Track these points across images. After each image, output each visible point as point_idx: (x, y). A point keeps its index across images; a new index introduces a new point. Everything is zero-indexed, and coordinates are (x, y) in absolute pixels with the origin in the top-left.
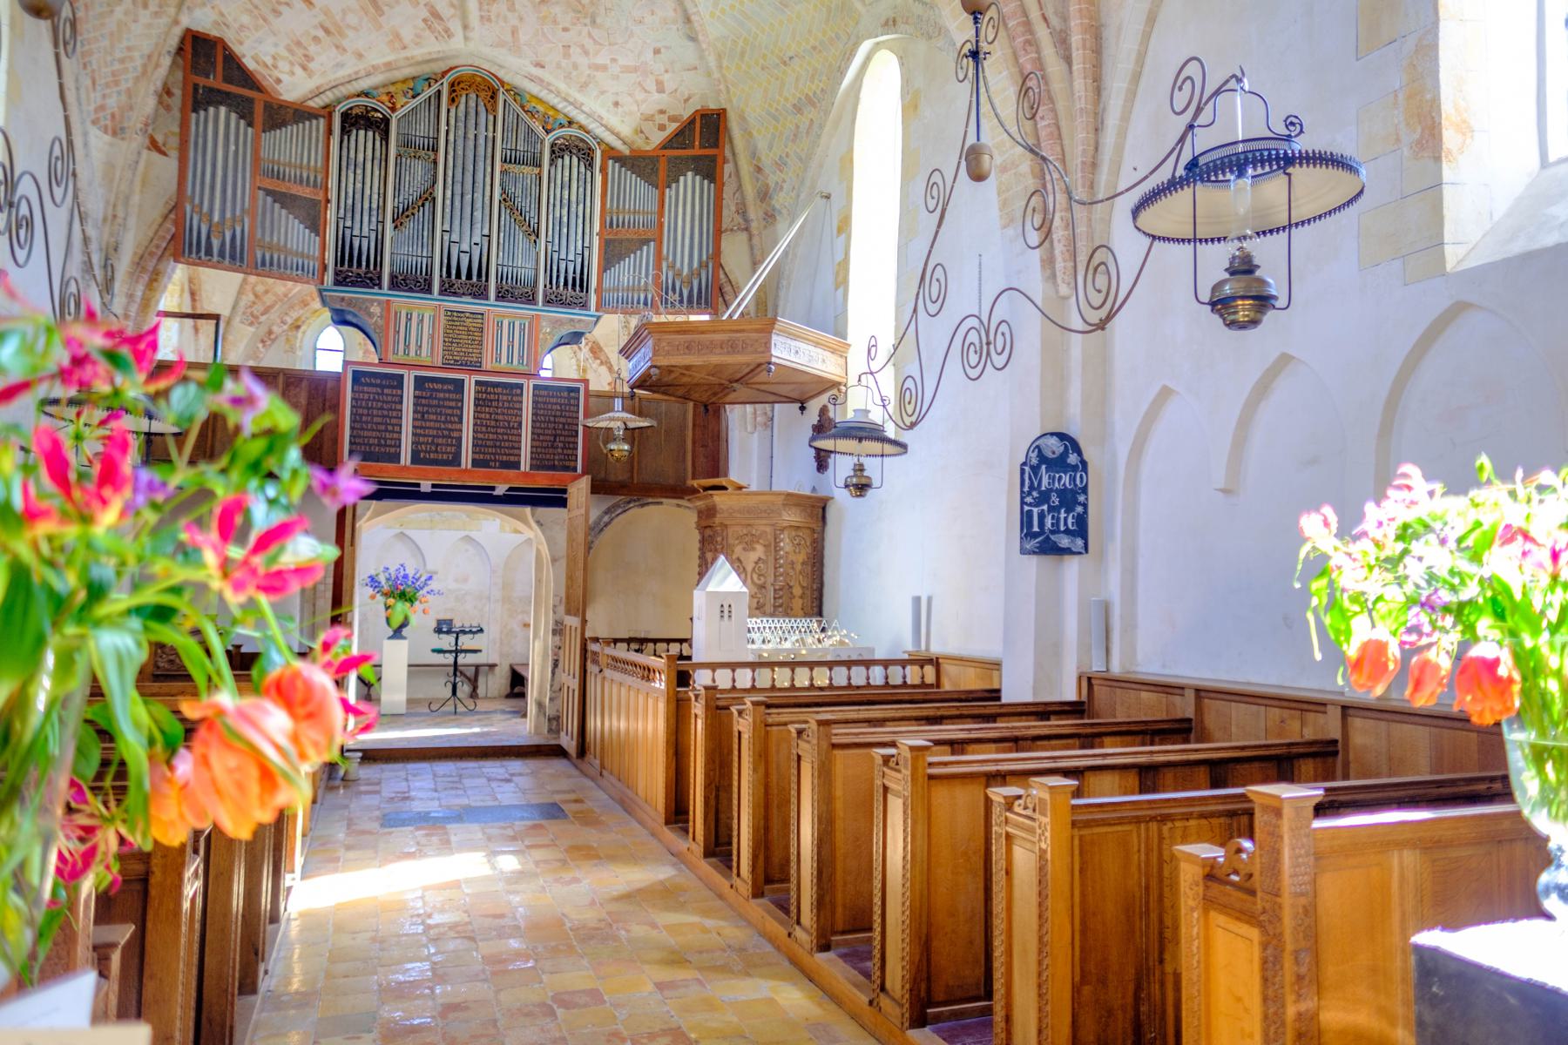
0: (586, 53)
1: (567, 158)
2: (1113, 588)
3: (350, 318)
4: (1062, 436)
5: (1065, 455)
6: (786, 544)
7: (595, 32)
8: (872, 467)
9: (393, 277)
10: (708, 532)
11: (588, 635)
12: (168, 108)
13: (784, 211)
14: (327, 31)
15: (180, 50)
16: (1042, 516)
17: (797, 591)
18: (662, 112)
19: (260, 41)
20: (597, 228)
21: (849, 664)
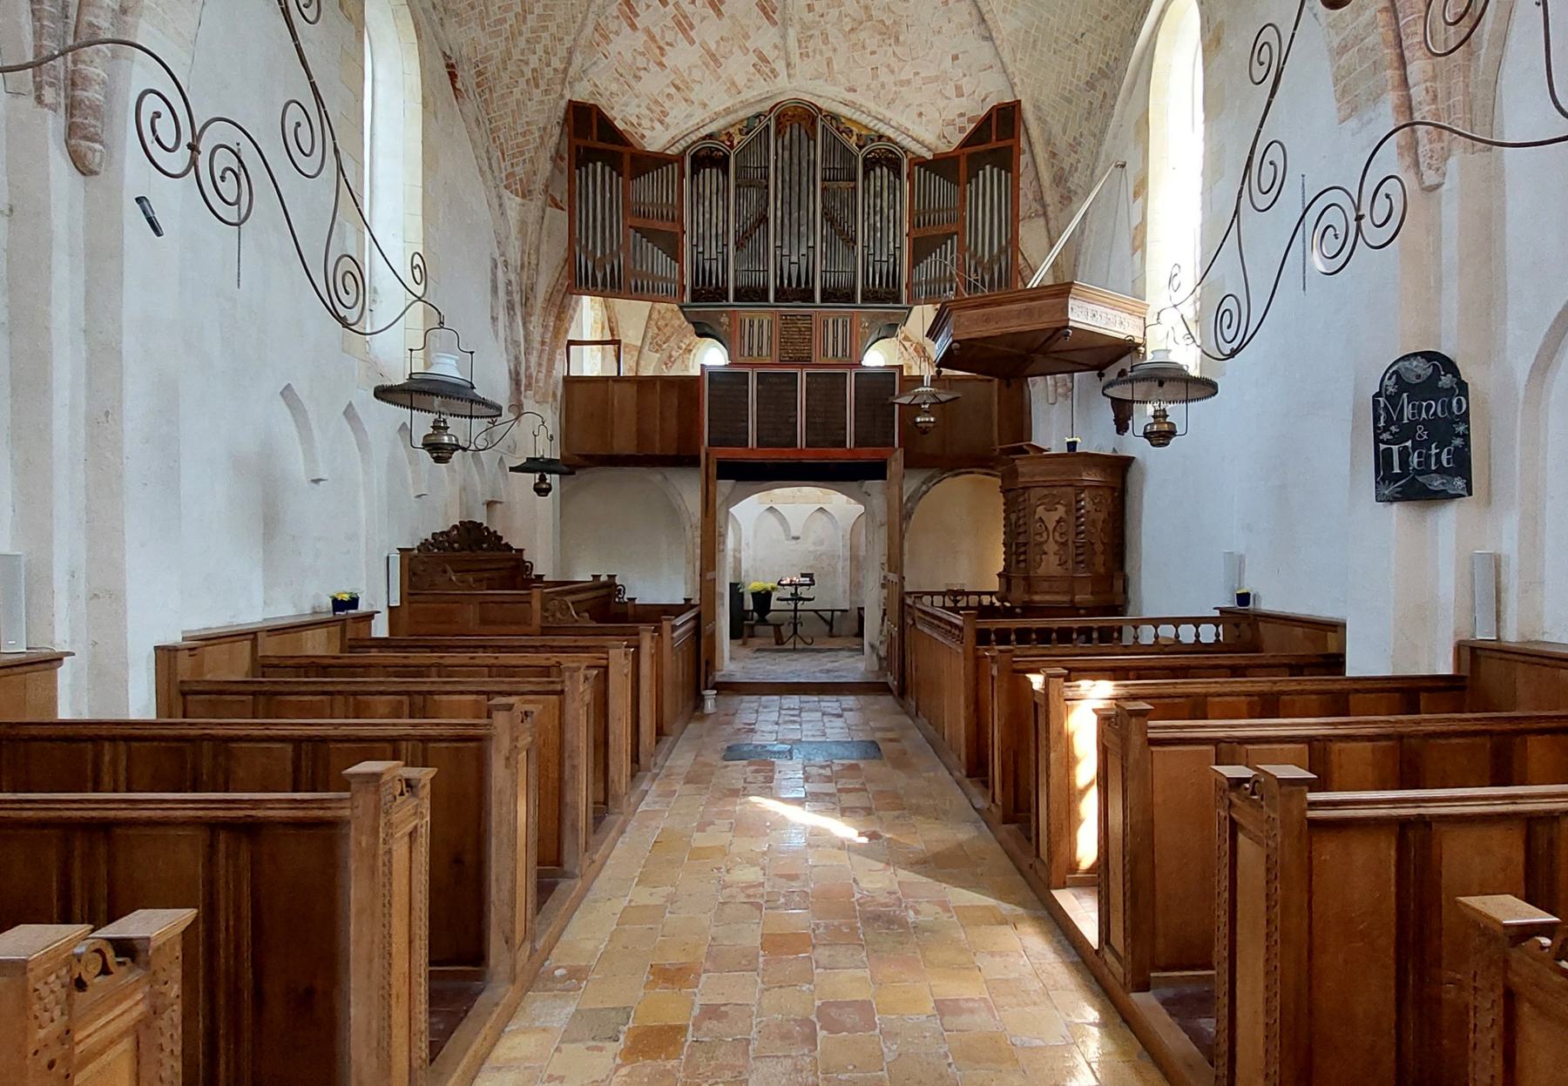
0: (892, 72)
1: (878, 170)
2: (1506, 537)
3: (707, 330)
4: (1428, 356)
5: (1435, 376)
6: (1086, 502)
7: (898, 50)
8: (1175, 412)
9: (736, 290)
10: (1011, 495)
11: (908, 589)
12: (562, 172)
13: (1080, 191)
14: (678, 88)
15: (566, 120)
16: (1404, 455)
17: (1099, 547)
18: (962, 115)
19: (626, 105)
20: (906, 229)
21: (1177, 622)
